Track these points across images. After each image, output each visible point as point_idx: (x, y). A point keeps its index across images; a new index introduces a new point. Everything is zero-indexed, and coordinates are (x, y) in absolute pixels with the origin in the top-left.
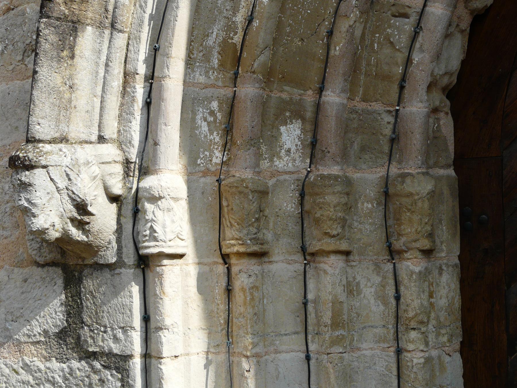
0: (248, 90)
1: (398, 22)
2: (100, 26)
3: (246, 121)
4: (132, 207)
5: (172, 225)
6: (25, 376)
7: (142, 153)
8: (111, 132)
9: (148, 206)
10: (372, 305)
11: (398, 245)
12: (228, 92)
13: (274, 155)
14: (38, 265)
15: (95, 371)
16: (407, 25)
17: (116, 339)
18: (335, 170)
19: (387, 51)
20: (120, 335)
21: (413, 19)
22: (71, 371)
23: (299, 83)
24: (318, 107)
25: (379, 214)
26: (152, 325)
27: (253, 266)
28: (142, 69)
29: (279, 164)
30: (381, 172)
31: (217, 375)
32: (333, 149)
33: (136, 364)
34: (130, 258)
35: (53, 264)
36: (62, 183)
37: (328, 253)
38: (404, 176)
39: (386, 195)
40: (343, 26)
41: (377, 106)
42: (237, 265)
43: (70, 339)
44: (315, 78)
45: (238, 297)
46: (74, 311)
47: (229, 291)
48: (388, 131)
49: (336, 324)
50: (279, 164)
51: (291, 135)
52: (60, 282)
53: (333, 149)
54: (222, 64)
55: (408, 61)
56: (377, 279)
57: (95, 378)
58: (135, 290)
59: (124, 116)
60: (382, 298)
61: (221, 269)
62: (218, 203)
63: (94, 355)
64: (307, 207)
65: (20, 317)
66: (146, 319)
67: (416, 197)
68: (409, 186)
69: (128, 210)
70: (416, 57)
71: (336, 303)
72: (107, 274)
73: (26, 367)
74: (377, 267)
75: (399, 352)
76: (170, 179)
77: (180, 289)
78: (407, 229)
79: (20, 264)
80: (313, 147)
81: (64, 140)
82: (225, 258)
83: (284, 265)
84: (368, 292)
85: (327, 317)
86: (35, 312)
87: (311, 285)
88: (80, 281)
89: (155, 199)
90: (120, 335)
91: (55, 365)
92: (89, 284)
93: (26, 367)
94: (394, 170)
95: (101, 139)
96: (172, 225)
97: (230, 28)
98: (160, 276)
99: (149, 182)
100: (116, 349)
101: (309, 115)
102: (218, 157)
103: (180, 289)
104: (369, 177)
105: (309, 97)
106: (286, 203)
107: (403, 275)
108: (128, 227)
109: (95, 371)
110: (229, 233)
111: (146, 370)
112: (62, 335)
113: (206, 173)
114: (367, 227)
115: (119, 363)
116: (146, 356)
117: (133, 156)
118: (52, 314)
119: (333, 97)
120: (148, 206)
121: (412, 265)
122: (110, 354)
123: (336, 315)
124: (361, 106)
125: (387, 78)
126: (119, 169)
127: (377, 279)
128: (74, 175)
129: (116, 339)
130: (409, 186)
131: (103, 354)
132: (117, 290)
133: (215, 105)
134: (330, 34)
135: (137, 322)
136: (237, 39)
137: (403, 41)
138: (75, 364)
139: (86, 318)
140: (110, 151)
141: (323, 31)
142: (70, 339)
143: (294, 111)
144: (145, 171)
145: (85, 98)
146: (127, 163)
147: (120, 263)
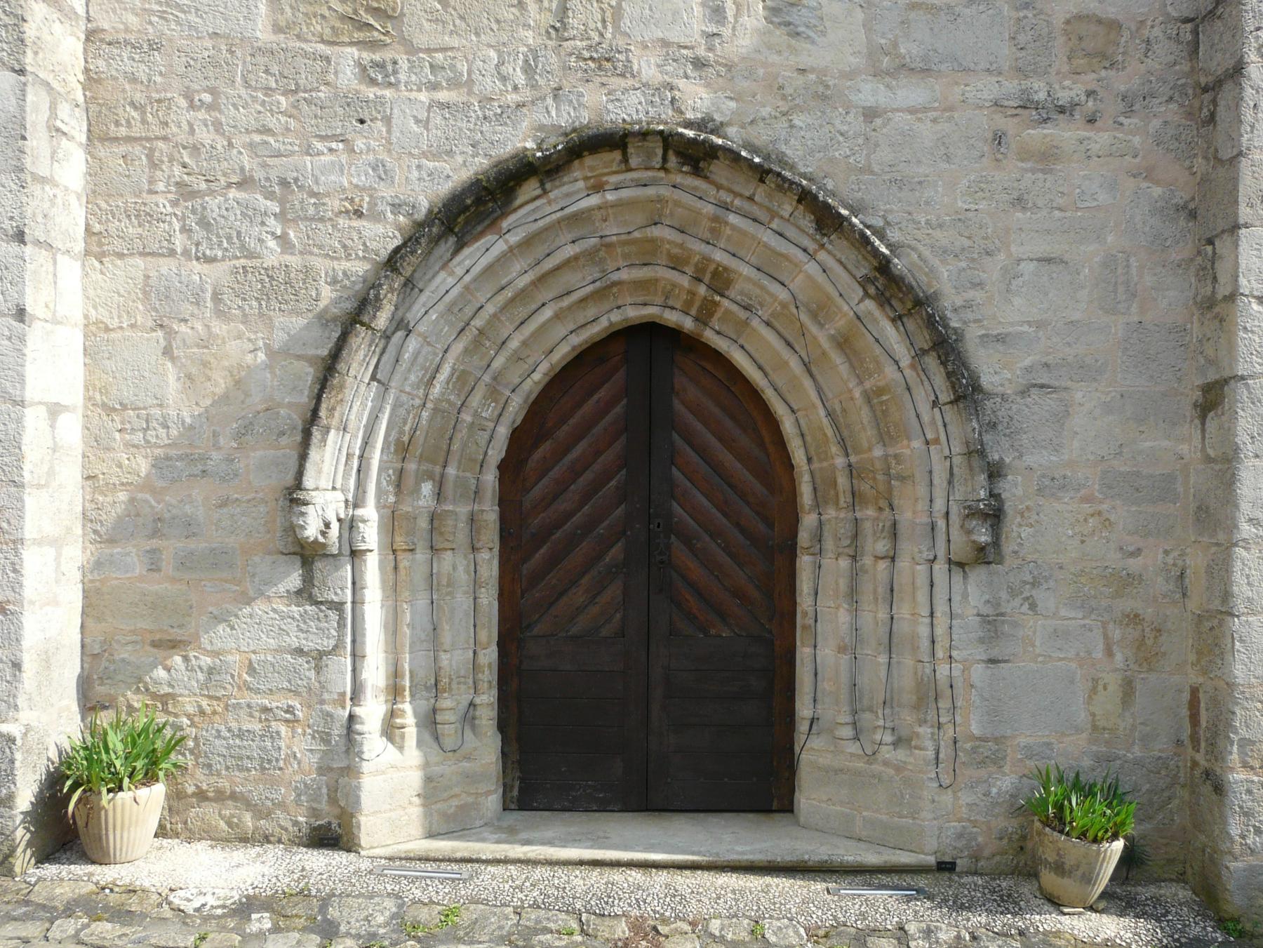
0: (411, 466)
1: (481, 433)
2: (338, 429)
3: (409, 481)
4: (350, 526)
5: (370, 535)
6: (272, 614)
7: (356, 496)
8: (338, 486)
9: (360, 525)
10: (462, 576)
11: (478, 545)
12: (399, 466)
13: (419, 498)
14: (283, 553)
15: (321, 611)
16: (486, 435)
17: (336, 594)
18: (451, 508)
19: (475, 447)
20: (339, 591)
21: (489, 432)
22: (306, 612)
23: (434, 463)
24: (442, 475)
25: (467, 530)
26: (358, 586)
27: (408, 555)
28: (357, 452)
29: (420, 503)
30: (470, 508)
31: (387, 612)
32: (451, 497)
33: (349, 606)
34: (346, 551)
35: (294, 554)
36: (320, 512)
37: (446, 549)
38: (483, 511)
39: (472, 519)
40: (458, 436)
41: (468, 474)
42: (401, 556)
43: (305, 594)
44: (442, 460)
45: (402, 572)
46: (308, 579)
47: (396, 568)
48: (473, 488)
49: (448, 586)
50: (420, 503)
51: (427, 488)
52: (299, 564)
53: (451, 497)
54: (396, 451)
55: (486, 453)
56: (465, 562)
57: (322, 615)
58: (349, 568)
59: (346, 476)
60: (468, 572)
61: (392, 557)
62: (392, 521)
63: (321, 603)
64: (435, 525)
65: (270, 583)
66: (354, 583)
67: (138, 438)
68: (485, 516)
69: (346, 526)
70: (490, 452)
71: (449, 574)
72: (331, 559)
73: (274, 610)
74: (465, 557)
75: (475, 599)
76: (370, 511)
77: (372, 567)
78: (483, 538)
79: (270, 553)
80: (439, 495)
81: (317, 489)
82: (394, 551)
83: (421, 556)
84: (461, 568)
85: (444, 582)
86: (281, 580)
87: (435, 565)
88: (313, 562)
89: (364, 521)
90: (339, 591)
91: (294, 608)
92: (319, 565)
93: (274, 610)
94: (476, 507)
95: (334, 488)
96: (370, 535)
97: (401, 432)
98: (365, 561)
99: (359, 512)
100: (336, 599)
101: (437, 478)
102: (392, 499)
103: (372, 567)
104: (463, 510)
105: (438, 469)
106: (423, 523)
107: (479, 560)
108: (346, 535)
109: (321, 611)
110: (398, 539)
111: (353, 610)
112: (299, 592)
113: (385, 506)
114: (462, 537)
115: (338, 607)
116: (353, 602)
117: (350, 499)
118: (294, 580)
119: (451, 471)
120: (360, 525)
121: (484, 555)
122: (332, 602)
123: (449, 579)
124: (461, 474)
125: (474, 461)
126: (343, 505)
127: (465, 562)
128: (323, 508)
129: (336, 594)
130: (485, 516)
131: (327, 602)
132: (337, 568)
133: (391, 472)
134: (451, 439)
135: (350, 585)
136: (406, 439)
137: (483, 443)
138: (308, 608)
139: (316, 583)
140: (339, 496)
141: (447, 437)
142: (305, 594)
143: (430, 476)
144: (356, 506)
145: (328, 467)
146: (347, 501)
147: (340, 554)
